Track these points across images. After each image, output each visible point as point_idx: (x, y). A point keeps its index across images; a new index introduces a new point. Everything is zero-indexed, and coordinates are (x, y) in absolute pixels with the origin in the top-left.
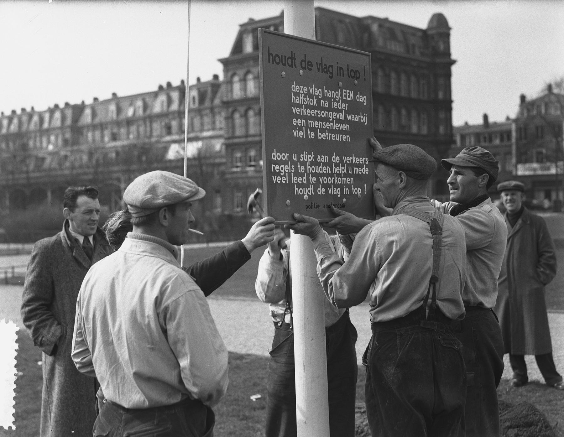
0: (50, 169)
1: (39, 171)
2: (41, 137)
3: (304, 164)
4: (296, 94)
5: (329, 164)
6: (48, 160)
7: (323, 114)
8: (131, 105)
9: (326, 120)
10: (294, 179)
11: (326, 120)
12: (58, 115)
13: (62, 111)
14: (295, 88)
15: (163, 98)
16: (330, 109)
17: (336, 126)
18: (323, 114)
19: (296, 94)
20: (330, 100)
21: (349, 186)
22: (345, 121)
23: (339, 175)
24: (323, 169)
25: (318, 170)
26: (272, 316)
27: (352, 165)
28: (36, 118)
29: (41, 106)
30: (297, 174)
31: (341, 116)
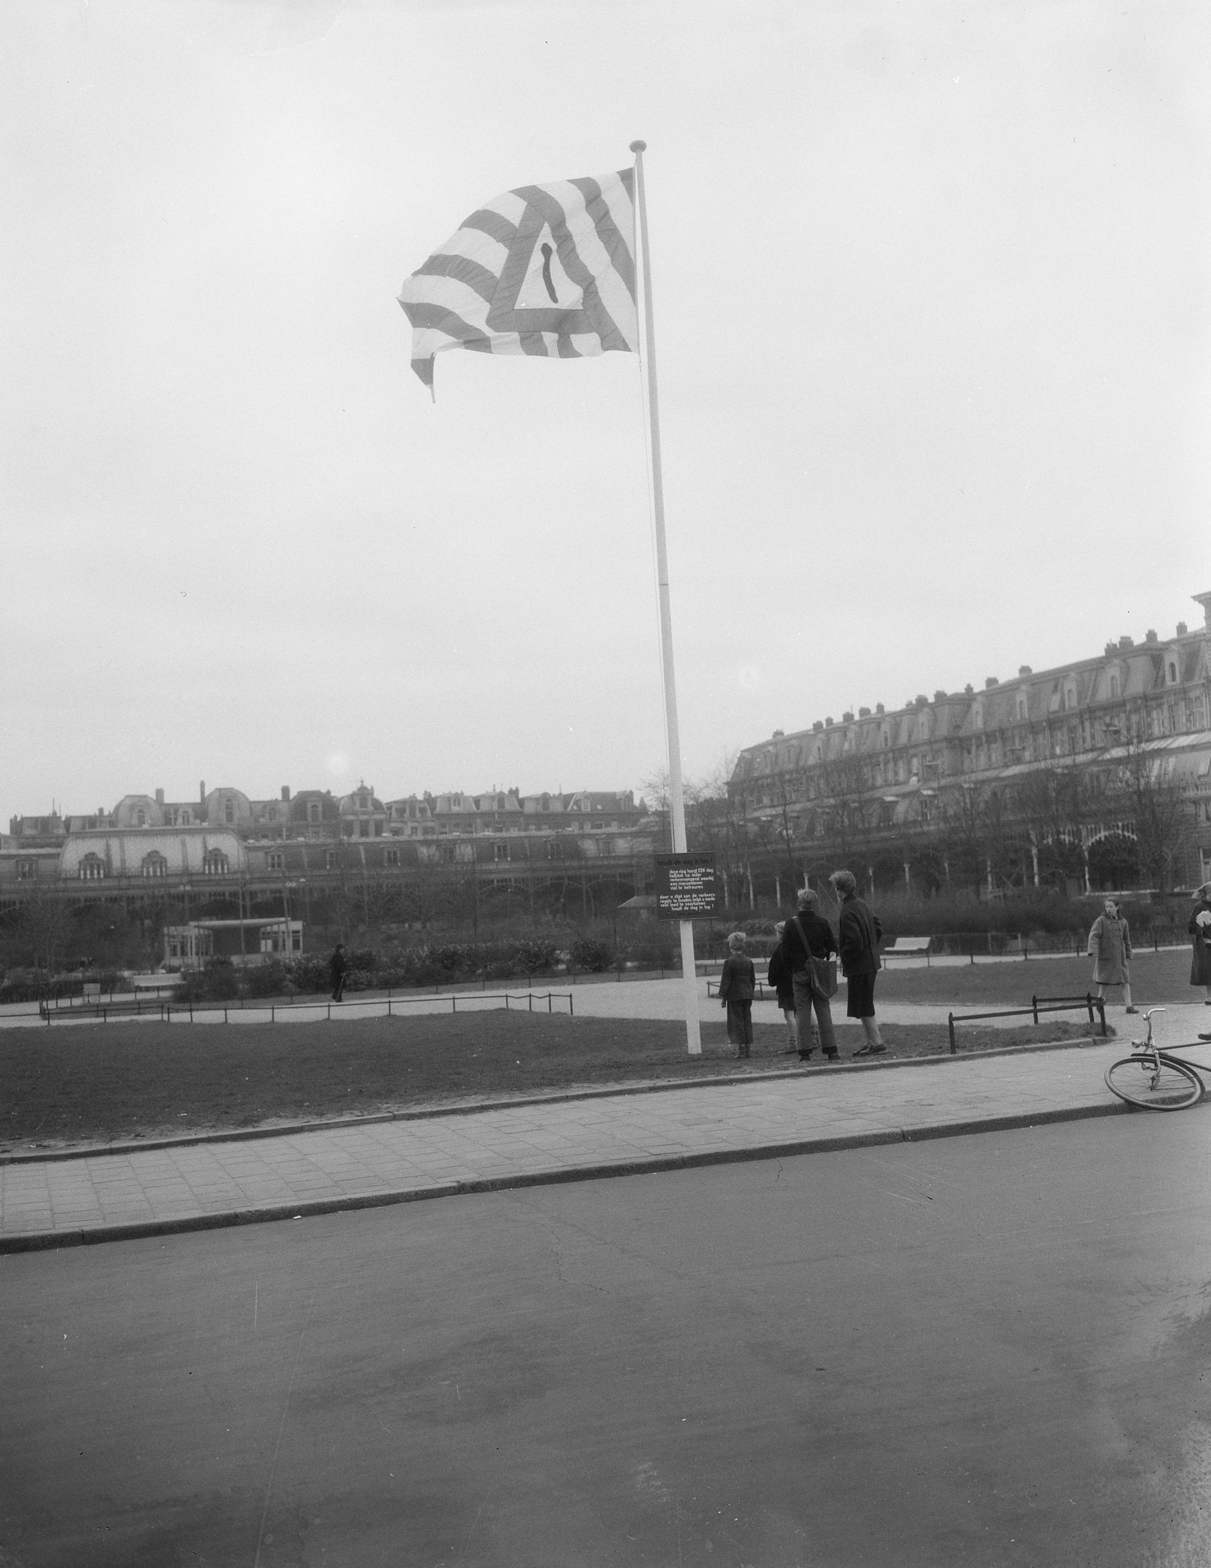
0: (906, 824)
1: (890, 828)
2: (896, 760)
3: (677, 899)
4: (672, 874)
5: (691, 898)
6: (901, 808)
7: (687, 880)
8: (1055, 690)
9: (689, 881)
10: (672, 905)
11: (689, 881)
12: (923, 718)
13: (933, 707)
14: (671, 872)
15: (1114, 671)
16: (691, 877)
17: (695, 883)
18: (687, 880)
19: (672, 874)
20: (691, 874)
21: (703, 906)
22: (700, 881)
23: (696, 902)
24: (687, 900)
25: (684, 901)
26: (394, 835)
27: (705, 897)
28: (885, 727)
29: (895, 704)
30: (673, 903)
31: (698, 879)
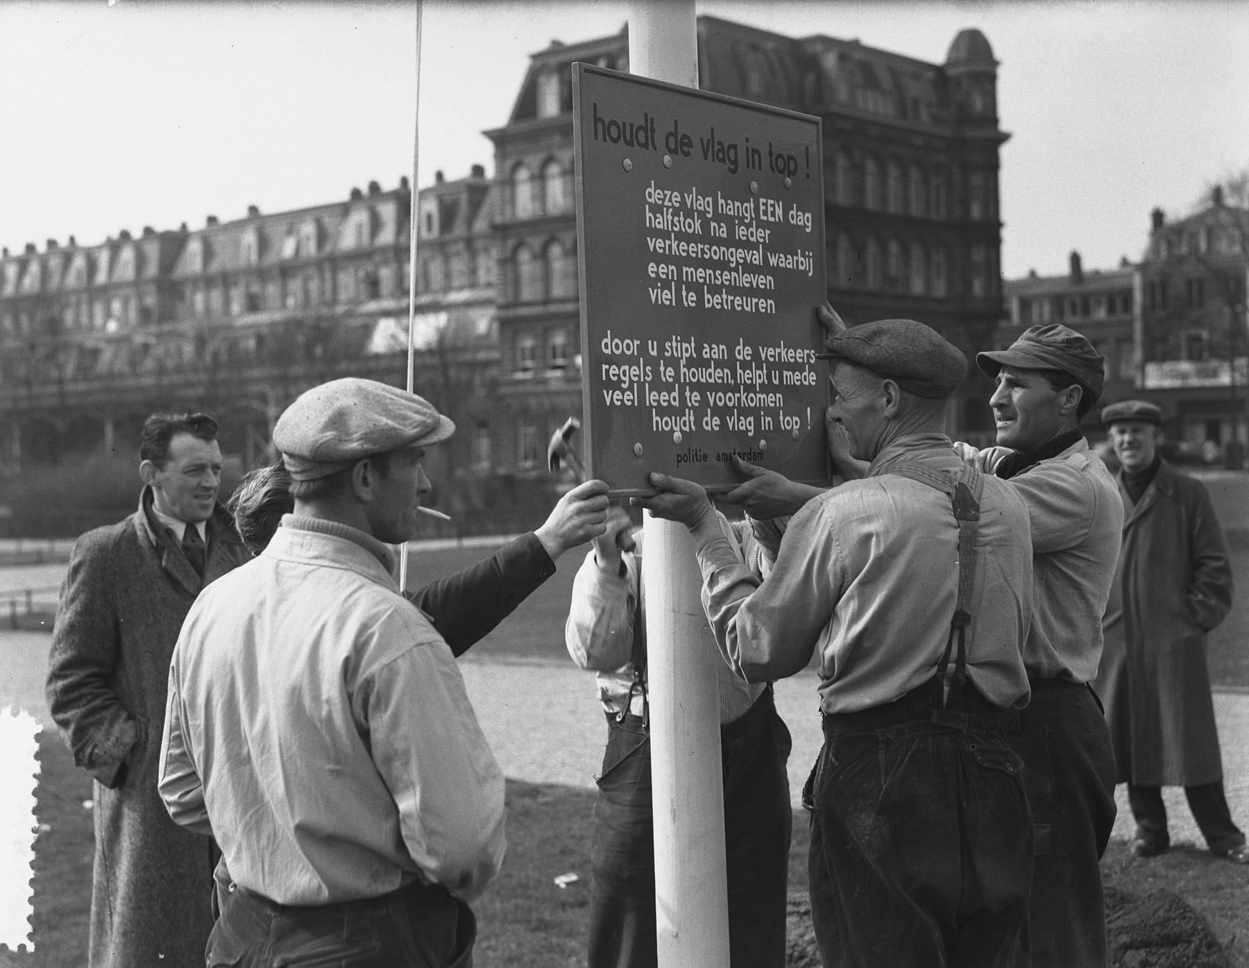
0: (111, 375)
1: (86, 379)
2: (91, 303)
3: (673, 362)
4: (656, 209)
5: (729, 363)
6: (107, 355)
7: (716, 253)
8: (290, 232)
9: (723, 265)
10: (652, 397)
11: (723, 265)
12: (127, 254)
13: (138, 247)
14: (654, 194)
15: (360, 217)
16: (731, 242)
17: (745, 280)
18: (716, 253)
19: (656, 209)
20: (730, 221)
21: (773, 412)
22: (765, 269)
23: (750, 388)
24: (716, 375)
25: (704, 376)
26: (602, 700)
27: (781, 366)
28: (79, 262)
29: (92, 236)
30: (658, 385)
31: (756, 258)
